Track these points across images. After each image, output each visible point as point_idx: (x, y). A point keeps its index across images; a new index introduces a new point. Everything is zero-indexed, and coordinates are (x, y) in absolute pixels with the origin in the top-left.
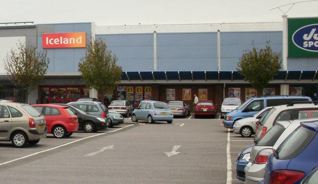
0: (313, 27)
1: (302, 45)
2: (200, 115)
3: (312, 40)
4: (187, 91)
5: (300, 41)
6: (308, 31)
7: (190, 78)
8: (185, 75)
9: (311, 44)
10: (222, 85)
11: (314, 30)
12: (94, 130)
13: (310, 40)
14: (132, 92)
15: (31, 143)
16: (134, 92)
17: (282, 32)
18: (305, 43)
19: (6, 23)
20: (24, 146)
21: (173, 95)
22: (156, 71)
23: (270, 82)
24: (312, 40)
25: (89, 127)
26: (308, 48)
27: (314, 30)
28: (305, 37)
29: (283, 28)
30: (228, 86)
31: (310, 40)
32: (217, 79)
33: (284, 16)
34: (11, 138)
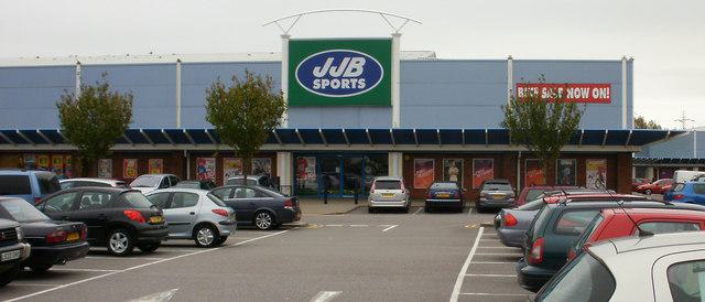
0: (331, 55)
1: (311, 86)
2: (436, 208)
3: (328, 76)
4: (131, 163)
5: (308, 78)
6: (320, 61)
7: (320, 141)
8: (450, 136)
9: (325, 83)
10: (517, 153)
11: (330, 60)
12: (275, 227)
13: (324, 78)
14: (47, 165)
15: (219, 241)
16: (50, 164)
17: (280, 63)
18: (315, 82)
19: (592, 86)
20: (128, 253)
21: (109, 171)
22: (398, 127)
23: (262, 148)
24: (328, 76)
25: (264, 222)
26: (320, 90)
27: (330, 60)
28: (316, 72)
29: (280, 53)
30: (194, 154)
31: (324, 78)
32: (484, 143)
33: (284, 37)
34: (195, 235)
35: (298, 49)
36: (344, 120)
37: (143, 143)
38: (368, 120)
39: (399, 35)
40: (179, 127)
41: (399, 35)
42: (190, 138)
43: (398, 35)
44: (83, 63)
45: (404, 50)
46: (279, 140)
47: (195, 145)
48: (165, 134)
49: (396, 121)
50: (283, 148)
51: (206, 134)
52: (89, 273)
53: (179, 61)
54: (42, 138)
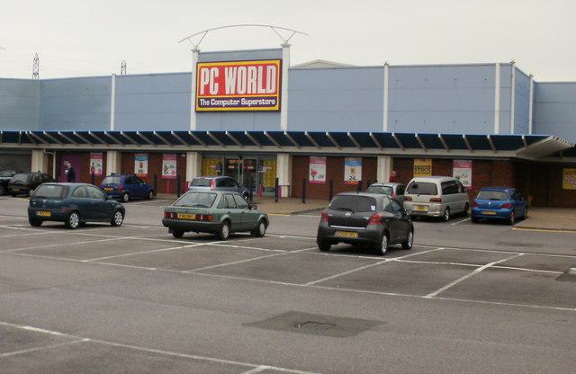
7: (441, 147)
22: (496, 133)
35: (204, 60)
36: (246, 125)
37: (195, 144)
38: (264, 125)
39: (288, 46)
40: (385, 130)
41: (288, 46)
42: (467, 144)
43: (286, 46)
44: (392, 63)
45: (295, 58)
46: (400, 144)
47: (449, 151)
48: (288, 136)
49: (284, 125)
50: (36, 147)
51: (415, 138)
52: (135, 263)
53: (386, 64)
54: (248, 139)
